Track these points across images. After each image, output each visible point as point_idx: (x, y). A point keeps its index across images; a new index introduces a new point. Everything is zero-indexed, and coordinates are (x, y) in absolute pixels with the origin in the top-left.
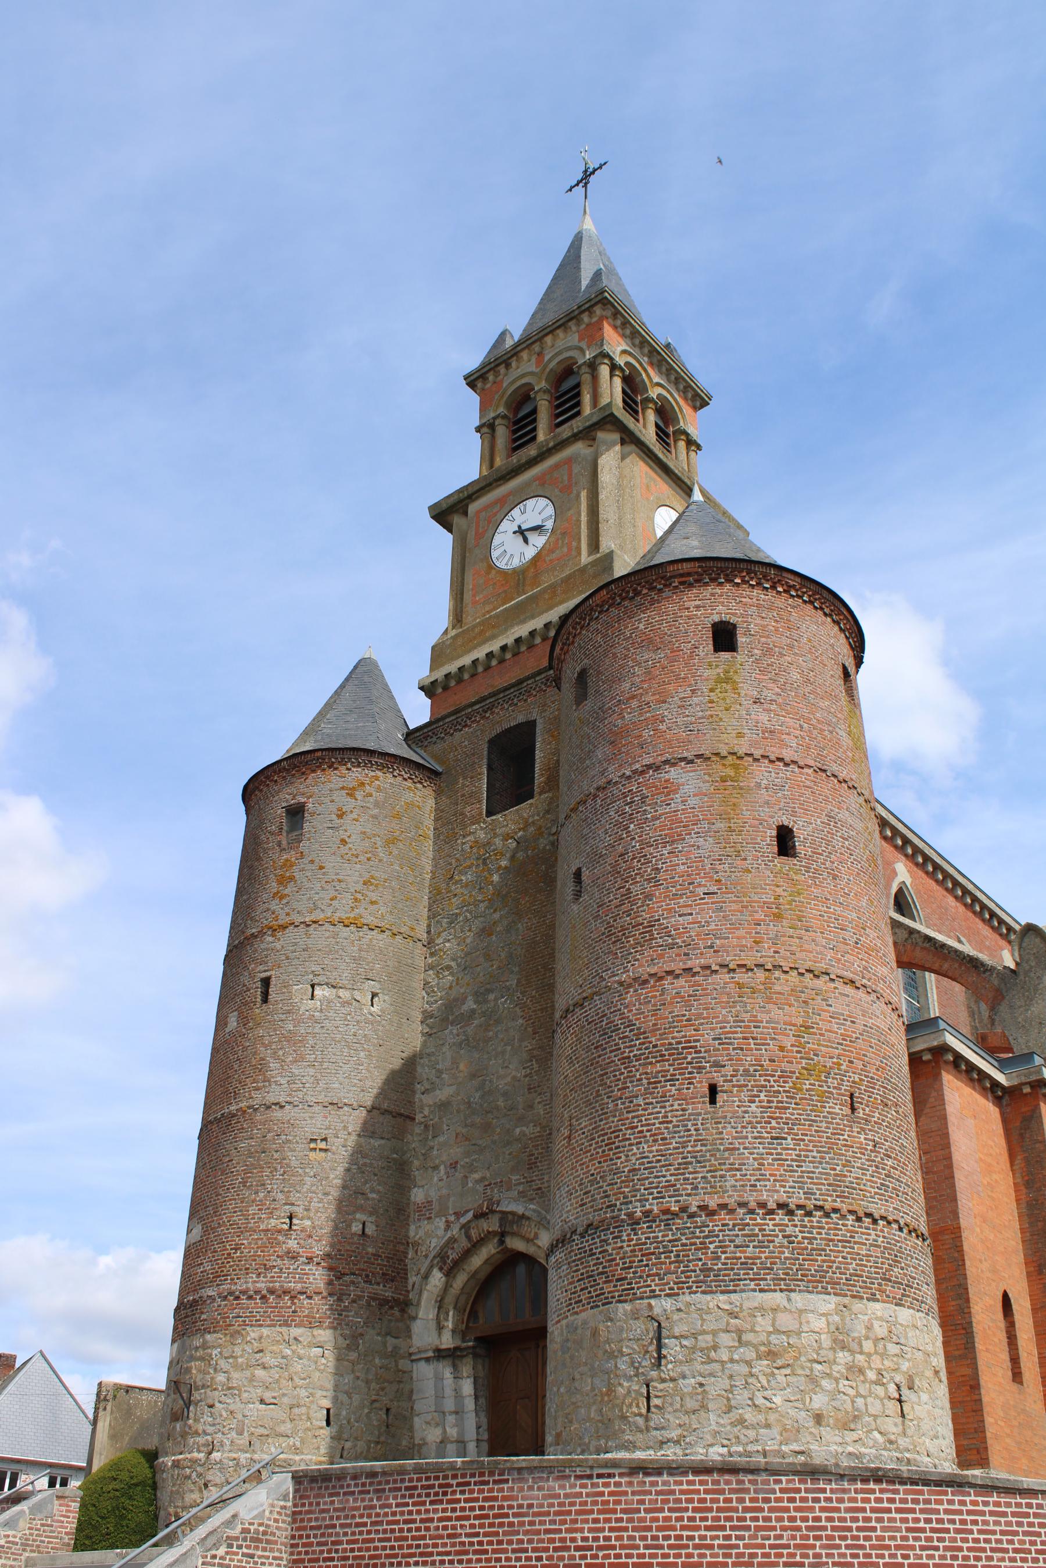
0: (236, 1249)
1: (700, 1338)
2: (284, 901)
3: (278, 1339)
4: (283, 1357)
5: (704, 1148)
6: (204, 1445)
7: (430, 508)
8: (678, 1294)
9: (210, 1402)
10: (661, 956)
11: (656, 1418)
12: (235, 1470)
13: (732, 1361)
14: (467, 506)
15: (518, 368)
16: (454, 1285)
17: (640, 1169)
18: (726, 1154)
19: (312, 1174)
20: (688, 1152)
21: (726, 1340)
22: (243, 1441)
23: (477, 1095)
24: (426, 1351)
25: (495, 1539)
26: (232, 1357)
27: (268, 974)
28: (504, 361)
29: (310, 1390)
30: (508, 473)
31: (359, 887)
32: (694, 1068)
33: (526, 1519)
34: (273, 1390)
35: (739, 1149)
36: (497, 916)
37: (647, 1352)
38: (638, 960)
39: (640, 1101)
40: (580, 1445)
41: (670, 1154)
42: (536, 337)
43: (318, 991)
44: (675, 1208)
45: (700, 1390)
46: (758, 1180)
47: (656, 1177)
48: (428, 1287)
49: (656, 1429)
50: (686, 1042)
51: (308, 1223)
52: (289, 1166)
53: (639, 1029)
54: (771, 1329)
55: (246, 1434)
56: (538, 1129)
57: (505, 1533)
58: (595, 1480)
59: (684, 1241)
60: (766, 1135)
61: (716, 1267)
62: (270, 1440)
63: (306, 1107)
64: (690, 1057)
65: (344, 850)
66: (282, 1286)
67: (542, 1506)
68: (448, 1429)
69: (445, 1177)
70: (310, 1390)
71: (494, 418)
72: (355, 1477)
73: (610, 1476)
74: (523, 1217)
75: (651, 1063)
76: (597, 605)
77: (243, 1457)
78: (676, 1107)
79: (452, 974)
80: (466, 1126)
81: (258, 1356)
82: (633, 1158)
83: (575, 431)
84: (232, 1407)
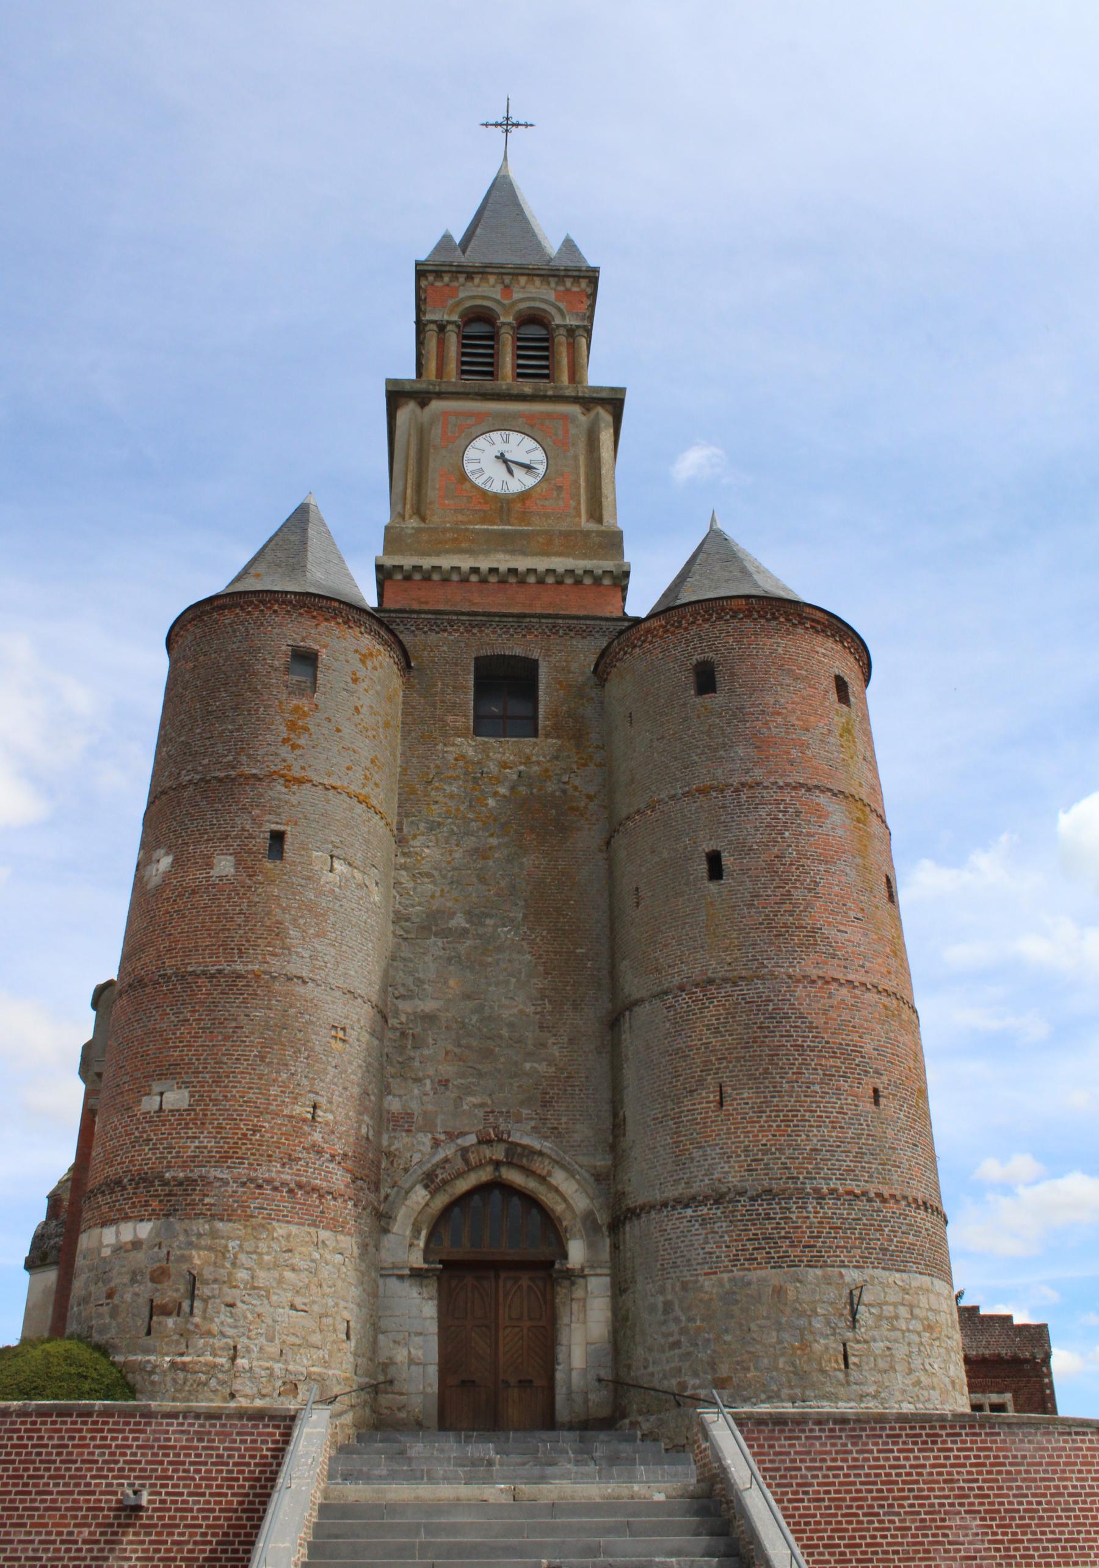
1: (884, 1307)
2: (298, 752)
3: (307, 1239)
6: (222, 1349)
7: (389, 382)
8: (863, 1267)
9: (229, 1300)
10: (826, 963)
11: (854, 1374)
12: (269, 1381)
13: (908, 1330)
14: (430, 399)
15: (478, 286)
18: (890, 1152)
21: (903, 1311)
22: (273, 1349)
23: (475, 1018)
25: (995, 1485)
26: (255, 1252)
27: (281, 828)
28: (468, 273)
30: (490, 394)
31: (368, 763)
33: (1022, 1468)
34: (304, 1295)
36: (494, 841)
37: (842, 1315)
39: (817, 1088)
40: (764, 1392)
42: (511, 271)
44: (858, 1191)
45: (887, 1353)
47: (837, 1160)
48: (408, 1202)
49: (856, 1384)
51: (330, 1117)
52: (312, 1049)
53: (810, 1023)
55: (277, 1341)
56: (553, 1069)
57: (1004, 1480)
58: (1074, 1437)
62: (302, 1351)
65: (357, 718)
66: (309, 1182)
67: (1034, 1457)
68: (412, 1351)
69: (431, 1093)
71: (449, 322)
72: (819, 1422)
73: (1084, 1434)
74: (541, 1153)
76: (731, 609)
77: (278, 1367)
78: (849, 1101)
79: (434, 883)
80: (460, 1046)
81: (287, 1255)
82: (815, 1140)
83: (580, 394)
84: (258, 1309)
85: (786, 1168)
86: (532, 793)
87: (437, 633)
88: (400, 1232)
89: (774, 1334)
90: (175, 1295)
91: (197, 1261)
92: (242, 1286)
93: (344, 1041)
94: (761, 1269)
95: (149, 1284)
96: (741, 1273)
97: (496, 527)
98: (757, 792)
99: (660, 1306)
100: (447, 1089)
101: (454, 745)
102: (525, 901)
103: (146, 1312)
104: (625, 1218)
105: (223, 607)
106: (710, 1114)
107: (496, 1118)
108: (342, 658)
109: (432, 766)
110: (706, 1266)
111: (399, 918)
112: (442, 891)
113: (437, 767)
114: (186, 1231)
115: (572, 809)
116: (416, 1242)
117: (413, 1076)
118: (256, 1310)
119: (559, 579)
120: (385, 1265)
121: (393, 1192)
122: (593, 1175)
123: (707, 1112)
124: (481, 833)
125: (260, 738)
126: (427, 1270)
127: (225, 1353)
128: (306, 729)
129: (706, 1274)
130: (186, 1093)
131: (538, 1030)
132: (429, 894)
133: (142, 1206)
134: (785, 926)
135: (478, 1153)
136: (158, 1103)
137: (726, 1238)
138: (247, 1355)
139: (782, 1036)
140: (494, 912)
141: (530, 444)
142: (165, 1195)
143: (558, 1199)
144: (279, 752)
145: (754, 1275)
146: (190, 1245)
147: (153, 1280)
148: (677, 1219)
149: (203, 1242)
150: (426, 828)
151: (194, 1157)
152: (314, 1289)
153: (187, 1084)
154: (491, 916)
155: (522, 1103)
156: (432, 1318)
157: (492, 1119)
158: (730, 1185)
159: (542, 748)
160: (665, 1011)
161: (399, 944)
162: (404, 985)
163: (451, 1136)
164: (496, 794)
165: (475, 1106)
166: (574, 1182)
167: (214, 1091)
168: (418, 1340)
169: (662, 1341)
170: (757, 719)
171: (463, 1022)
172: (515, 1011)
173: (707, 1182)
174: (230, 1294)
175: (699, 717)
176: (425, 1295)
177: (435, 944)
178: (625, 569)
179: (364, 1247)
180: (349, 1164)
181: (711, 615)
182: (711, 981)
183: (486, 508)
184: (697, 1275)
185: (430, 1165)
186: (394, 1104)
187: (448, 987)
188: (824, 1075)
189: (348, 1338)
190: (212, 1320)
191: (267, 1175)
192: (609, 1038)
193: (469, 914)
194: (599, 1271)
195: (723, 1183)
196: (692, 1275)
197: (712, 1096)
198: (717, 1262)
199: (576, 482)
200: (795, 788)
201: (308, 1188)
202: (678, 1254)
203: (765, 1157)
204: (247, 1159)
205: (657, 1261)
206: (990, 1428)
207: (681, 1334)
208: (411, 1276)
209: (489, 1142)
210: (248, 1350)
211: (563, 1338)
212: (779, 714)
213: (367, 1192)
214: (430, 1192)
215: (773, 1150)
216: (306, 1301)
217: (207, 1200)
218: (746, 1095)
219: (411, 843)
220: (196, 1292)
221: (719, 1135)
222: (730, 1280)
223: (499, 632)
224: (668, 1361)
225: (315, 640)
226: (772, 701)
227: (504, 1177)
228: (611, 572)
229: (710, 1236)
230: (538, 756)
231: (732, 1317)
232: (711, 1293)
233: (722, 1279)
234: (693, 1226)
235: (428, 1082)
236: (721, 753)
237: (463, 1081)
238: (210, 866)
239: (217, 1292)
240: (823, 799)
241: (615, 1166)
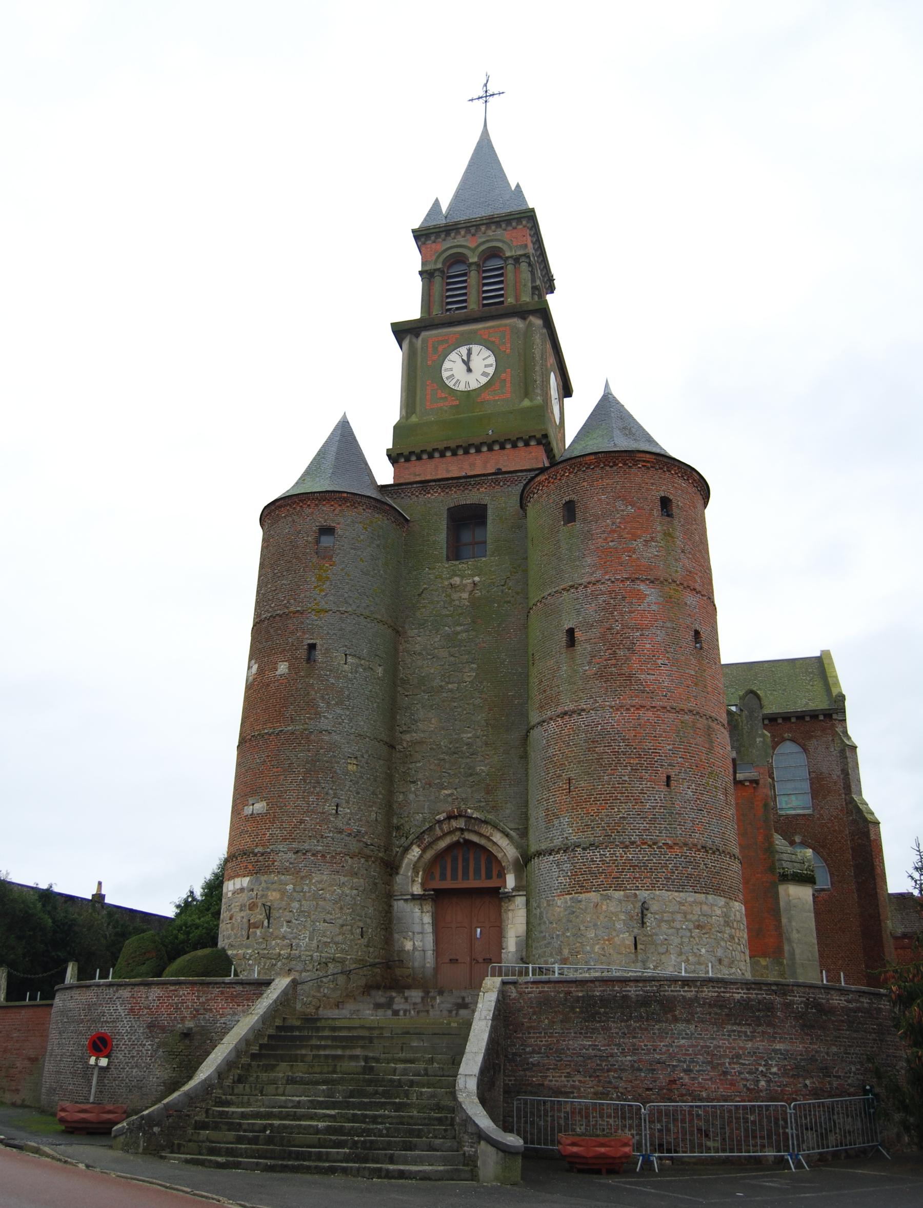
3: (333, 883)
5: (665, 811)
15: (454, 238)
16: (425, 856)
17: (627, 818)
18: (677, 816)
20: (656, 812)
21: (679, 917)
26: (302, 891)
32: (659, 765)
35: (683, 814)
38: (622, 695)
41: (646, 812)
43: (350, 659)
46: (693, 832)
50: (654, 749)
52: (335, 772)
54: (700, 913)
59: (655, 861)
60: (695, 808)
61: (672, 878)
64: (656, 758)
68: (416, 942)
75: (633, 758)
78: (648, 786)
95: (248, 911)
103: (246, 926)
105: (280, 507)
116: (416, 879)
125: (301, 587)
133: (244, 869)
139: (605, 746)
142: (255, 862)
146: (268, 888)
147: (250, 909)
151: (269, 839)
156: (429, 923)
178: (543, 433)
181: (574, 469)
184: (554, 896)
188: (632, 769)
194: (521, 893)
196: (552, 896)
203: (592, 823)
206: (674, 987)
209: (456, 817)
214: (421, 849)
215: (597, 818)
231: (571, 921)
234: (553, 866)
236: (577, 563)
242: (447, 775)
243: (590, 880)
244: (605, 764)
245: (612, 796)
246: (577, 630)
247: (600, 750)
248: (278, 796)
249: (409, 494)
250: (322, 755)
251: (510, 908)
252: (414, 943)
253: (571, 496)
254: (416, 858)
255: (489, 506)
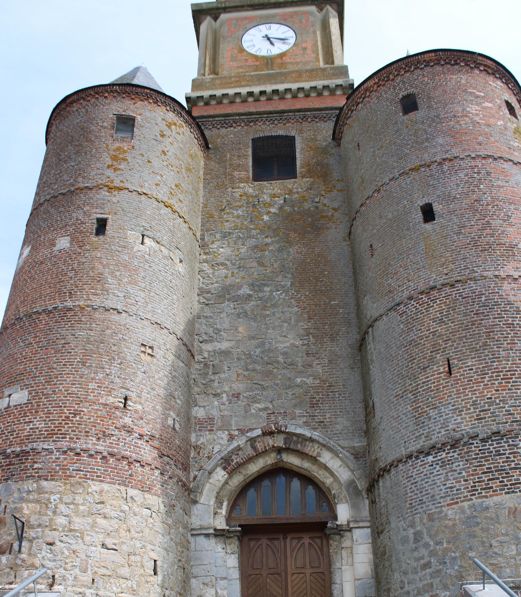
0: (75, 414)
2: (118, 172)
3: (117, 495)
4: (122, 511)
7: (192, 5)
9: (50, 540)
16: (230, 483)
19: (143, 370)
22: (87, 578)
23: (258, 351)
24: (208, 528)
26: (73, 503)
27: (105, 216)
29: (143, 543)
36: (269, 240)
48: (210, 481)
51: (139, 407)
55: (89, 572)
56: (318, 381)
62: (112, 580)
63: (138, 319)
66: (120, 452)
68: (219, 591)
69: (227, 403)
70: (143, 543)
76: (424, 61)
79: (227, 269)
80: (247, 370)
81: (99, 506)
84: (74, 547)
85: (510, 414)
86: (294, 210)
87: (226, 128)
88: (206, 503)
89: (514, 547)
90: (9, 538)
91: (26, 511)
92: (60, 529)
93: (152, 356)
94: (497, 495)
96: (480, 500)
97: (264, 72)
98: (456, 162)
99: (411, 536)
100: (239, 400)
101: (239, 188)
102: (292, 274)
104: (379, 476)
106: (442, 382)
107: (276, 418)
108: (153, 122)
109: (224, 201)
110: (448, 499)
111: (202, 292)
112: (233, 273)
113: (228, 201)
114: (19, 489)
115: (323, 217)
116: (219, 511)
117: (214, 393)
118: (72, 547)
119: (307, 93)
120: (194, 526)
121: (199, 474)
122: (352, 454)
123: (439, 381)
124: (259, 236)
126: (228, 530)
127: (45, 581)
128: (125, 160)
129: (448, 505)
130: (26, 392)
131: (305, 356)
132: (224, 275)
134: (488, 243)
135: (263, 442)
136: (7, 403)
137: (464, 474)
138: (63, 583)
139: (495, 318)
140: (269, 283)
141: (284, 28)
143: (328, 475)
144: (105, 172)
145: (490, 502)
146: (22, 499)
148: (421, 465)
149: (31, 497)
150: (220, 236)
152: (123, 533)
153: (27, 386)
154: (268, 286)
155: (295, 406)
157: (273, 418)
158: (463, 432)
159: (300, 184)
160: (399, 317)
161: (203, 308)
162: (206, 333)
163: (242, 432)
164: (269, 213)
165: (260, 410)
166: (338, 460)
167: (46, 388)
168: (223, 583)
169: (415, 564)
170: (451, 120)
171: (249, 354)
172: (288, 344)
173: (443, 433)
174: (51, 535)
175: (407, 127)
176: (229, 551)
177: (228, 306)
178: (350, 82)
179: (171, 508)
180: (156, 443)
181: (411, 67)
182: (433, 288)
183: (258, 63)
184: (441, 507)
185: (226, 452)
186: (199, 413)
187: (238, 332)
189: (155, 574)
190: (35, 556)
191: (84, 446)
192: (359, 358)
193: (252, 285)
194: (361, 524)
195: (457, 432)
196: (436, 508)
197: (441, 368)
198: (457, 494)
199: (316, 44)
200: (484, 158)
201: (119, 457)
202: (424, 493)
204: (69, 434)
205: (406, 501)
207: (430, 556)
208: (216, 536)
209: (271, 433)
210: (64, 578)
211: (337, 578)
212: (466, 116)
213: (173, 467)
214: (227, 472)
215: (498, 401)
216: (116, 541)
217: (36, 466)
218: (470, 364)
219: (211, 246)
220: (24, 535)
221: (451, 396)
222: (470, 507)
223: (268, 123)
224: (421, 580)
225: (133, 111)
226: (460, 109)
227: (285, 460)
228: (342, 85)
229: (449, 474)
230: (297, 188)
231: (475, 536)
232: (455, 520)
233: (464, 507)
234: (435, 468)
235: (224, 395)
237: (250, 394)
238: (54, 245)
239: (40, 534)
240: (507, 166)
241: (369, 445)
242: (260, 387)
243: (498, 478)
244: (499, 337)
245: (515, 374)
246: (436, 204)
247: (488, 322)
248: (46, 382)
249: (210, 127)
250: (108, 335)
251: (343, 546)
252: (216, 590)
253: (409, 91)
254: (221, 483)
255: (296, 137)
